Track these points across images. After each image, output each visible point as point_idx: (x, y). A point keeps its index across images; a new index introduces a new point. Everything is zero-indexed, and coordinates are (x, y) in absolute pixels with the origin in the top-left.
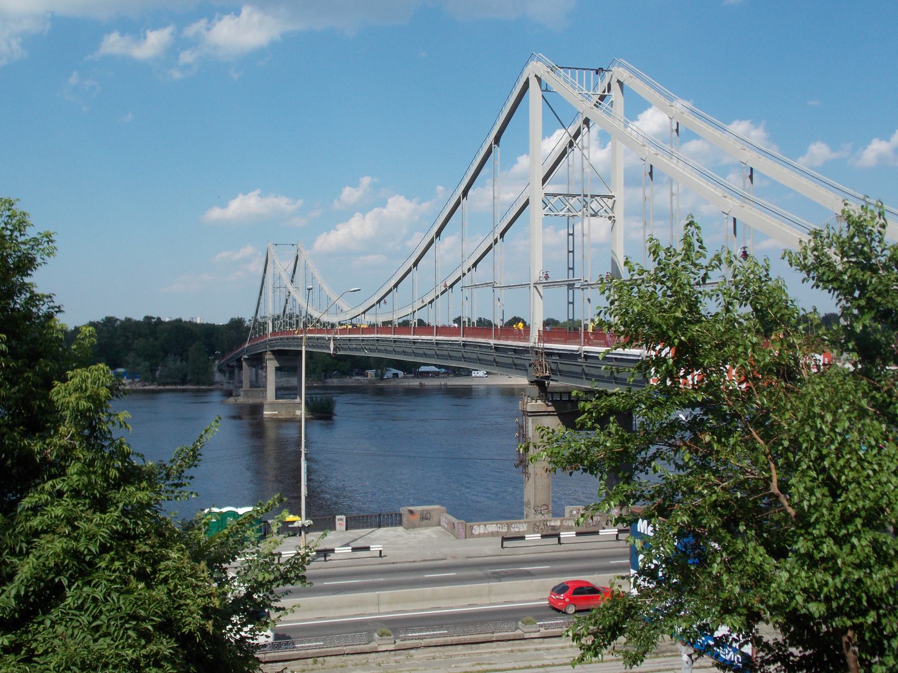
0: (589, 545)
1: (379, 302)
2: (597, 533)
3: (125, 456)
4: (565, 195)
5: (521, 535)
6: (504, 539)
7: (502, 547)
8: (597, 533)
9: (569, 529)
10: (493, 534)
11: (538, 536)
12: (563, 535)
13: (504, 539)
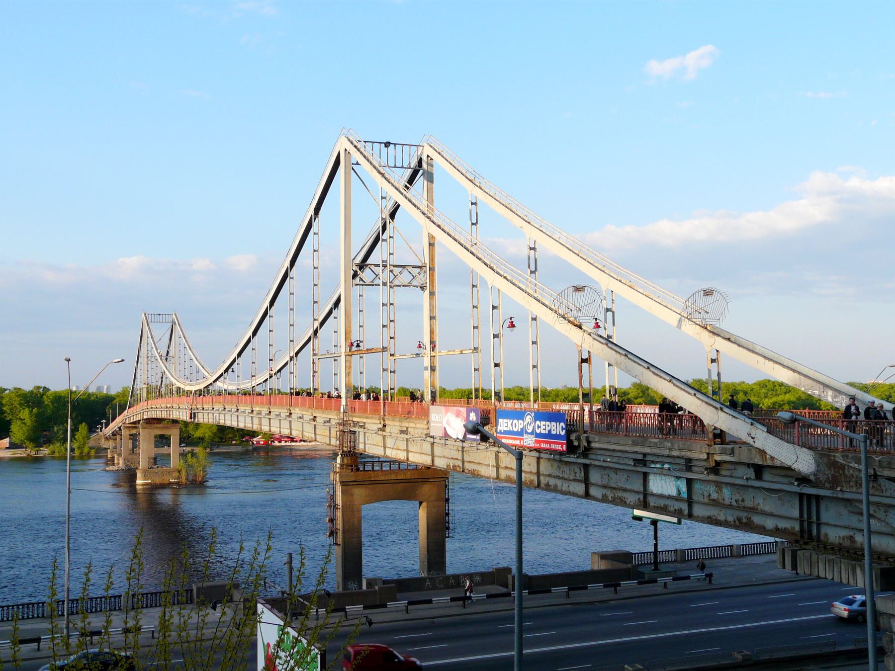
1: (226, 370)
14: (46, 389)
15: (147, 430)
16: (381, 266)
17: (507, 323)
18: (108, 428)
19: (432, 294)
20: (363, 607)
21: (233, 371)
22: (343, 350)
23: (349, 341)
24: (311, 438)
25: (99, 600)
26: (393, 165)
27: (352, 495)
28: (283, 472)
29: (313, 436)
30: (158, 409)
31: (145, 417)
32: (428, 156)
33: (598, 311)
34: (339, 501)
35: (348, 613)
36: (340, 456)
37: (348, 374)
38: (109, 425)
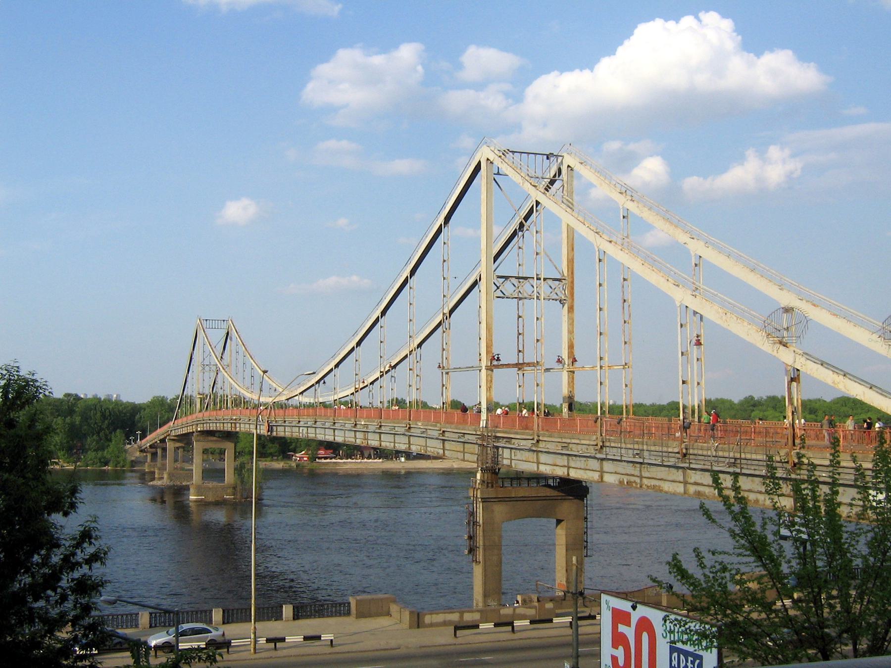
0: (544, 632)
1: (318, 382)
2: (551, 621)
3: (109, 551)
4: (516, 278)
5: (474, 624)
6: (457, 628)
7: (455, 635)
8: (551, 621)
9: (523, 617)
10: (445, 623)
11: (490, 625)
12: (517, 623)
13: (457, 628)
14: (77, 398)
15: (199, 443)
16: (542, 279)
17: (694, 341)
18: (145, 440)
19: (571, 309)
20: (494, 625)
21: (324, 383)
22: (484, 363)
23: (491, 355)
24: (438, 453)
25: (125, 617)
26: (496, 172)
27: (493, 511)
28: (364, 490)
29: (441, 452)
30: (220, 421)
31: (199, 429)
32: (569, 166)
33: (804, 331)
34: (480, 519)
35: (515, 628)
36: (480, 472)
37: (489, 389)
38: (146, 437)
